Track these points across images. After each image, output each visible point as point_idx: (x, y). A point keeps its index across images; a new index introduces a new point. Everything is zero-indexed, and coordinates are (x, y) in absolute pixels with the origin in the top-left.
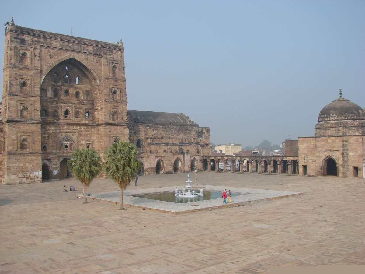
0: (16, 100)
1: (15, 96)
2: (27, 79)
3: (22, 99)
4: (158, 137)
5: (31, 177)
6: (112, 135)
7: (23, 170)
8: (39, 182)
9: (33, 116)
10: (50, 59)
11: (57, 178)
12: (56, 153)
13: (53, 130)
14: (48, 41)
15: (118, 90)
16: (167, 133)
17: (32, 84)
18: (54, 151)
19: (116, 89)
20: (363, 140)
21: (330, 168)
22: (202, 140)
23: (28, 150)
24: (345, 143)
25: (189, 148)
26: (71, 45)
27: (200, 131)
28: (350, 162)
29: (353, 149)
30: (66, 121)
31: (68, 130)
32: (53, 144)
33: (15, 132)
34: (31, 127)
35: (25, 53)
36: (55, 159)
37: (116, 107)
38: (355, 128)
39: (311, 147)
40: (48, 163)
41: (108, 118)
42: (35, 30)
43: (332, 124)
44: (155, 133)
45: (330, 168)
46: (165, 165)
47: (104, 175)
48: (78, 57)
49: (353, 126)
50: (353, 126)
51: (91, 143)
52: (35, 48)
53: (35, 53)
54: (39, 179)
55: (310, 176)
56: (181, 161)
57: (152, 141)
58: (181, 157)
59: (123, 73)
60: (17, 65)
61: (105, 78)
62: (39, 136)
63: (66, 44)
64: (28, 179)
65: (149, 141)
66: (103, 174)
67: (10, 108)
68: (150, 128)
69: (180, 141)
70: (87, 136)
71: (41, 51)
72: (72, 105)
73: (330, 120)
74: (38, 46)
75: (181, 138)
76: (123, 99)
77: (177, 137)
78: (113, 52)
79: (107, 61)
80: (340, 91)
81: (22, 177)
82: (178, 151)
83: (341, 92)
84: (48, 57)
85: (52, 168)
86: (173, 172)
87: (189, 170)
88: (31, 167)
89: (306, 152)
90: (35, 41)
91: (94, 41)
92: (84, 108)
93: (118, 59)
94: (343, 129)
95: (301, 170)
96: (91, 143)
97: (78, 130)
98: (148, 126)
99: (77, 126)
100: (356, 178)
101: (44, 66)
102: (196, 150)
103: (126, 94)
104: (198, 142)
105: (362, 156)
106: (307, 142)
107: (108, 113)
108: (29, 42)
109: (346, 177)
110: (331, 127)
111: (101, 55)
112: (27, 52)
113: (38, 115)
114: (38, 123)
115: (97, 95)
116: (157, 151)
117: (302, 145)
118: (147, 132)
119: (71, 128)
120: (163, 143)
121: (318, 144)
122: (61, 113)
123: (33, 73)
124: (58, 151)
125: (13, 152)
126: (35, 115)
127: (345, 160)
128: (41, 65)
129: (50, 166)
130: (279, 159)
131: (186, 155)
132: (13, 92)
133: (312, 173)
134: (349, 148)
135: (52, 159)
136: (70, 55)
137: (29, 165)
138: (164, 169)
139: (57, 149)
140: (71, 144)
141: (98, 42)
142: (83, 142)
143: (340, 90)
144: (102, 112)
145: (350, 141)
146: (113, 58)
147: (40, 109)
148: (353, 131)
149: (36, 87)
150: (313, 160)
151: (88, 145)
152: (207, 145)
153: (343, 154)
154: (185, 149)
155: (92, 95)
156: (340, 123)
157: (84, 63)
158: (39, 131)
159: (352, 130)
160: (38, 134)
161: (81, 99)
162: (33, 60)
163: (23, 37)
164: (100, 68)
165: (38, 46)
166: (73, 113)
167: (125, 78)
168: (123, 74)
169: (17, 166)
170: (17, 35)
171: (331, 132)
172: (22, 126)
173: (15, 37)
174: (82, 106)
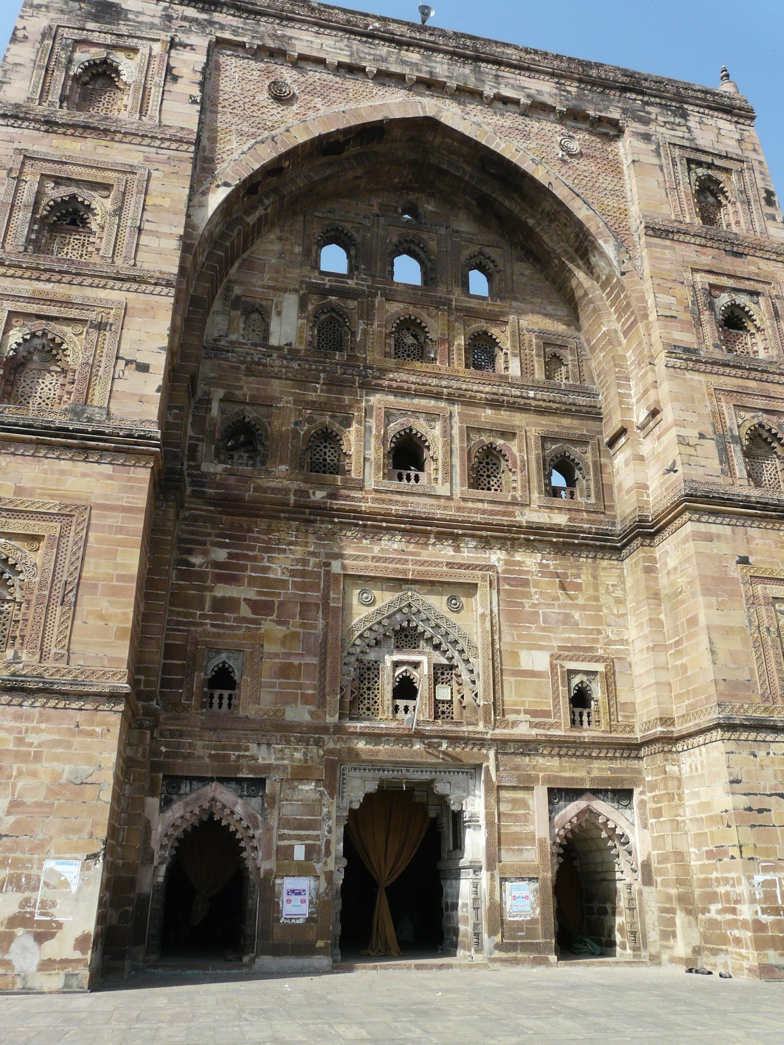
2: (94, 186)
3: (26, 287)
8: (56, 981)
11: (307, 949)
12: (313, 734)
13: (298, 561)
14: (266, 26)
15: (757, 303)
18: (299, 714)
30: (405, 503)
31: (415, 562)
32: (288, 655)
34: (62, 472)
36: (301, 774)
40: (236, 807)
41: (714, 464)
47: (738, 941)
48: (451, 114)
53: (172, 64)
54: (63, 946)
60: (41, 110)
61: (656, 231)
62: (124, 543)
63: (383, 49)
66: (733, 924)
70: (567, 619)
71: (209, 75)
72: (443, 404)
74: (201, 41)
78: (685, 115)
79: (654, 147)
84: (264, 97)
85: (267, 856)
93: (721, 148)
96: (600, 667)
97: (491, 567)
99: (486, 543)
107: (708, 429)
111: (614, 123)
112: (119, 58)
122: (363, 446)
123: (147, 159)
124: (332, 719)
129: (258, 833)
135: (276, 776)
139: (321, 701)
140: (441, 673)
142: (538, 661)
147: (159, 362)
149: (152, 233)
151: (576, 680)
155: (580, 362)
160: (120, 530)
162: (155, 94)
174: (519, 419)
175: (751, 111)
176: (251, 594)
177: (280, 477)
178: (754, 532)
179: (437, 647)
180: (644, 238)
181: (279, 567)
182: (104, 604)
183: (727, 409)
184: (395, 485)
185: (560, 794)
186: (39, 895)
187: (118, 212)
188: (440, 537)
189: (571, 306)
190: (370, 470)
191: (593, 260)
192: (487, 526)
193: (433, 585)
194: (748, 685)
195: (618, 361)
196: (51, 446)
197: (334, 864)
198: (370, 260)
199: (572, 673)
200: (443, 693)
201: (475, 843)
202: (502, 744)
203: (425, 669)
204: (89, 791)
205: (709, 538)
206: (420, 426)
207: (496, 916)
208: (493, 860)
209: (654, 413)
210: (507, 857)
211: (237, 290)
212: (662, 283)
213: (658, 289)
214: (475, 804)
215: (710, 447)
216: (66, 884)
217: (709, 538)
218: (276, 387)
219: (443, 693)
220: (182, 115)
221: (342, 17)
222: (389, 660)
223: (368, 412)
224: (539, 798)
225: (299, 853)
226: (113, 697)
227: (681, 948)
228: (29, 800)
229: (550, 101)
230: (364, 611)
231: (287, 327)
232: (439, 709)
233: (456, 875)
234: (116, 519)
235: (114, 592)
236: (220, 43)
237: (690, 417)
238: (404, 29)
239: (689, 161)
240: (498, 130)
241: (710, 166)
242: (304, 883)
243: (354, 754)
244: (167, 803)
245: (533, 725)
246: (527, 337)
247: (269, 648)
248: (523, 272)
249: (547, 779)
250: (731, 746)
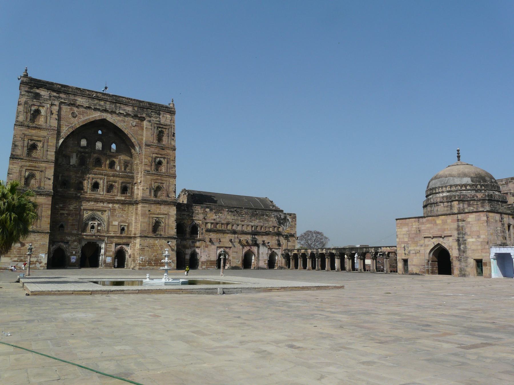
0: (20, 164)
2: (38, 141)
3: (28, 164)
4: (223, 222)
6: (151, 215)
8: (42, 268)
9: (42, 185)
10: (73, 119)
14: (72, 97)
16: (235, 218)
17: (45, 147)
18: (75, 232)
20: (487, 218)
21: (442, 262)
22: (285, 229)
24: (461, 224)
25: (266, 238)
26: (102, 103)
27: (282, 217)
28: (469, 253)
29: (479, 234)
36: (75, 241)
37: (160, 181)
38: (479, 203)
39: (413, 232)
40: (64, 246)
42: (55, 83)
43: (443, 197)
44: (218, 217)
45: (442, 262)
46: (231, 258)
48: (109, 118)
49: (475, 200)
50: (475, 200)
51: (127, 224)
52: (52, 105)
55: (413, 274)
57: (212, 227)
58: (255, 249)
59: (173, 140)
60: (26, 123)
61: (147, 145)
63: (96, 102)
65: (209, 226)
69: (253, 229)
70: (122, 216)
71: (60, 109)
73: (439, 193)
74: (57, 103)
75: (254, 225)
76: (171, 171)
77: (249, 224)
78: (159, 114)
80: (457, 152)
81: (17, 261)
82: (250, 242)
83: (458, 154)
84: (70, 116)
87: (266, 266)
89: (406, 240)
90: (54, 96)
91: (134, 100)
92: (120, 181)
93: (166, 123)
94: (459, 204)
95: (400, 265)
96: (127, 224)
98: (207, 207)
99: (109, 203)
100: (480, 278)
101: (64, 126)
102: (276, 242)
103: (174, 166)
104: (280, 232)
105: (488, 243)
106: (407, 224)
107: (148, 187)
108: (45, 97)
109: (464, 275)
110: (441, 202)
112: (41, 108)
113: (50, 185)
114: (47, 195)
115: (137, 165)
116: (220, 239)
117: (401, 230)
118: (207, 215)
120: (229, 230)
121: (423, 227)
122: (87, 185)
124: (80, 233)
127: (462, 249)
128: (59, 125)
130: (373, 251)
131: (261, 248)
132: (17, 155)
133: (415, 270)
134: (467, 230)
136: (101, 116)
139: (78, 230)
140: (99, 225)
141: (140, 102)
142: (116, 223)
143: (458, 151)
145: (469, 220)
146: (159, 121)
147: (52, 178)
148: (475, 206)
149: (50, 151)
150: (420, 255)
152: (292, 236)
153: (458, 240)
154: (260, 239)
156: (455, 196)
157: (120, 125)
159: (473, 205)
161: (116, 170)
162: (49, 118)
163: (38, 91)
164: (143, 134)
167: (174, 146)
168: (172, 141)
170: (29, 88)
171: (441, 208)
173: (26, 90)
174: (117, 179)
176: (67, 212)
177: (72, 191)
178: (152, 206)
181: (72, 207)
182: (46, 219)
183: (153, 183)
184: (93, 192)
185: (117, 244)
187: (43, 147)
188: (101, 202)
189: (131, 156)
190: (89, 189)
192: (110, 200)
193: (99, 211)
194: (145, 231)
195: (137, 169)
197: (79, 254)
198: (91, 144)
200: (99, 228)
201: (102, 251)
202: (108, 237)
205: (144, 207)
206: (98, 181)
207: (105, 262)
208: (105, 254)
210: (107, 254)
211: (64, 153)
213: (145, 158)
214: (103, 246)
215: (148, 190)
217: (144, 207)
218: (71, 173)
219: (99, 228)
220: (54, 123)
221: (88, 93)
222: (90, 223)
223: (89, 178)
224: (113, 245)
225: (74, 253)
226: (48, 233)
227: (132, 267)
229: (130, 113)
230: (86, 215)
231: (74, 161)
232: (98, 231)
233: (100, 256)
234: (46, 206)
235: (47, 217)
236: (61, 103)
237: (146, 185)
238: (101, 95)
240: (119, 120)
241: (162, 128)
242: (75, 257)
243: (83, 238)
244: (53, 245)
246: (122, 161)
247: (70, 221)
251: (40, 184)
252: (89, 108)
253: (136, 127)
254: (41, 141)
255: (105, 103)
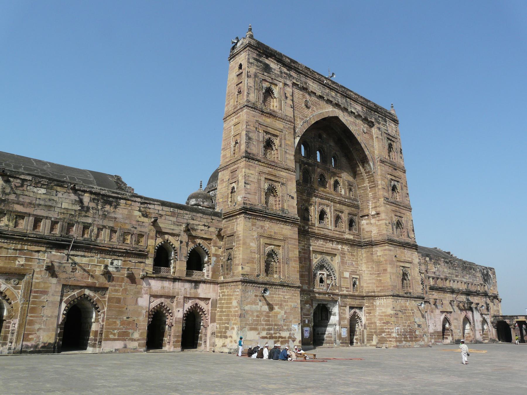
1: (257, 162)
5: (282, 338)
7: (268, 321)
10: (306, 110)
17: (283, 146)
19: (396, 183)
23: (275, 276)
33: (255, 234)
34: (282, 228)
35: (269, 88)
44: (437, 269)
46: (453, 328)
48: (344, 118)
56: (470, 323)
59: (401, 158)
61: (382, 162)
64: (278, 341)
67: (248, 184)
68: (430, 259)
81: (266, 338)
86: (497, 340)
88: (283, 314)
91: (361, 97)
96: (358, 277)
99: (338, 243)
108: (276, 72)
111: (372, 123)
112: (273, 87)
119: (330, 245)
125: (252, 278)
126: (288, 206)
131: (475, 312)
132: (254, 155)
137: (279, 310)
138: (452, 335)
144: (378, 221)
147: (295, 196)
157: (352, 128)
158: (295, 239)
163: (267, 61)
165: (289, 83)
166: (331, 217)
169: (257, 311)
170: (257, 54)
172: (267, 224)
175: (398, 121)
178: (397, 249)
179: (328, 270)
180: (379, 163)
185: (351, 308)
186: (292, 332)
187: (281, 146)
188: (330, 241)
191: (365, 165)
193: (328, 254)
196: (280, 221)
199: (353, 278)
202: (341, 295)
203: (325, 275)
204: (297, 309)
209: (378, 214)
212: (383, 178)
216: (296, 330)
224: (347, 308)
225: (307, 322)
226: (298, 287)
228: (287, 311)
229: (361, 114)
235: (295, 261)
239: (388, 138)
245: (347, 291)
248: (344, 160)
249: (349, 304)
250: (393, 300)
251: (283, 205)
252: (321, 97)
253: (366, 135)
254: (277, 136)
255: (336, 95)
